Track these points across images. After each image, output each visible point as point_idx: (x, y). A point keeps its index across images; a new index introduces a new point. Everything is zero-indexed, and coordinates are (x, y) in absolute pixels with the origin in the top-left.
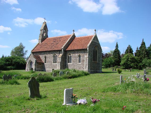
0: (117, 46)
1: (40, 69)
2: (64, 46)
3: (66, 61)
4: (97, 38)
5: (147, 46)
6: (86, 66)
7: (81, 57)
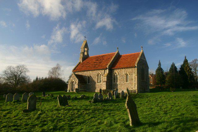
0: (160, 64)
1: (83, 89)
2: (109, 64)
3: (111, 80)
4: (144, 55)
5: (197, 62)
6: (135, 85)
7: (129, 75)
